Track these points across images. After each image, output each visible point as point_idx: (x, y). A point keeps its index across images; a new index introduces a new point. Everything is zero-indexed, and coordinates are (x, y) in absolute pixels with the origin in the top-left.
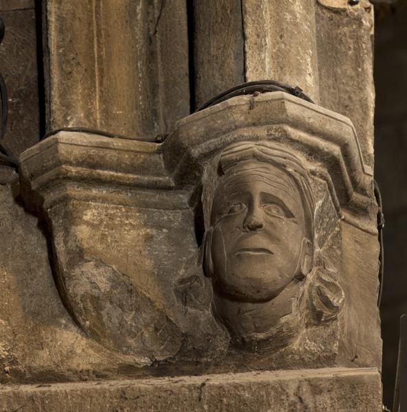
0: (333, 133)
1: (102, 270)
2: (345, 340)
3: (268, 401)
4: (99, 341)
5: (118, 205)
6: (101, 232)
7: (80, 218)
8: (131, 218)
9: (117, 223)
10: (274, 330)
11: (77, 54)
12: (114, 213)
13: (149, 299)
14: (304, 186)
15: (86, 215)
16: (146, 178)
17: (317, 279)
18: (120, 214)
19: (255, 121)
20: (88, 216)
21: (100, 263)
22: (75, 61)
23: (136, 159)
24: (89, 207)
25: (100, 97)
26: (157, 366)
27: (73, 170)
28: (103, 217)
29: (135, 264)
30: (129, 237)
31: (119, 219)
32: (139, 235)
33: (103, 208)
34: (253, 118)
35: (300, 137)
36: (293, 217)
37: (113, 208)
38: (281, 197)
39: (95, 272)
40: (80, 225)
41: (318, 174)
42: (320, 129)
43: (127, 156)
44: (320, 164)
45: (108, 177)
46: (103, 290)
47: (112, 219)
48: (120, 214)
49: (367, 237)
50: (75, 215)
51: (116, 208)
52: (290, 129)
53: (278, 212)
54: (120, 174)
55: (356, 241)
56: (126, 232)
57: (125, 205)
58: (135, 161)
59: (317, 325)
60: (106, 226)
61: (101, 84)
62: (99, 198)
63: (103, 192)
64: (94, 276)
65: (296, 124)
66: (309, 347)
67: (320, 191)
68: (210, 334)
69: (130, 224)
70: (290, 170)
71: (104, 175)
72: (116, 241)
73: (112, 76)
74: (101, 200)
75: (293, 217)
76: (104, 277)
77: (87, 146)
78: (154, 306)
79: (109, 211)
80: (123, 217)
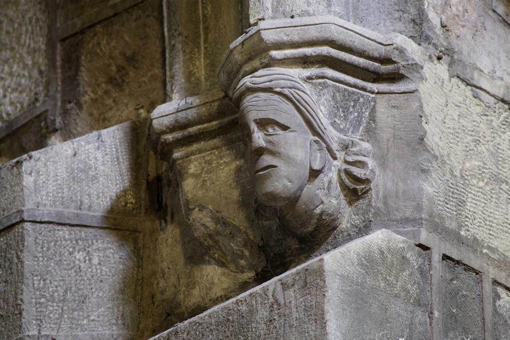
0: (314, 39)
1: (204, 212)
2: (380, 205)
3: (256, 308)
4: (227, 267)
5: (212, 150)
6: (202, 179)
7: (187, 173)
8: (224, 157)
9: (214, 165)
10: (314, 221)
11: (178, 25)
12: (211, 158)
13: (235, 225)
14: (295, 97)
15: (190, 169)
16: (226, 120)
17: (344, 162)
18: (215, 158)
19: (249, 56)
20: (192, 169)
21: (202, 208)
22: (177, 32)
23: (211, 108)
24: (190, 161)
25: (205, 54)
26: (260, 276)
27: (169, 137)
28: (203, 164)
29: (226, 198)
30: (223, 174)
31: (215, 162)
32: (230, 170)
33: (200, 158)
34: (246, 55)
35: (285, 55)
36: (289, 128)
37: (208, 155)
38: (272, 117)
39: (201, 216)
40: (187, 179)
41: (314, 77)
42: (302, 40)
43: (204, 109)
44: (317, 66)
45: (197, 132)
46: (211, 228)
47: (211, 164)
48: (215, 158)
49: (405, 97)
50: (183, 172)
51: (211, 154)
52: (275, 53)
53: (274, 130)
54: (205, 125)
55: (393, 107)
56: (221, 171)
57: (217, 148)
58: (211, 110)
59: (358, 200)
60: (207, 172)
61: (206, 41)
62: (196, 151)
63: (202, 145)
64: (202, 219)
65: (279, 46)
66: (354, 221)
67: (321, 90)
68: (280, 239)
69: (225, 162)
70: (278, 90)
71: (193, 131)
72: (213, 183)
73: (222, 27)
74: (198, 152)
75: (289, 128)
76: (208, 217)
77: (173, 113)
78: (241, 230)
79: (206, 159)
80: (218, 160)
